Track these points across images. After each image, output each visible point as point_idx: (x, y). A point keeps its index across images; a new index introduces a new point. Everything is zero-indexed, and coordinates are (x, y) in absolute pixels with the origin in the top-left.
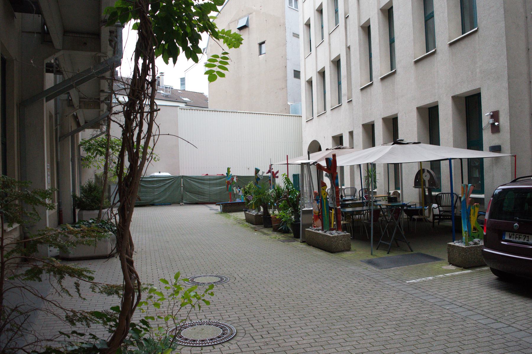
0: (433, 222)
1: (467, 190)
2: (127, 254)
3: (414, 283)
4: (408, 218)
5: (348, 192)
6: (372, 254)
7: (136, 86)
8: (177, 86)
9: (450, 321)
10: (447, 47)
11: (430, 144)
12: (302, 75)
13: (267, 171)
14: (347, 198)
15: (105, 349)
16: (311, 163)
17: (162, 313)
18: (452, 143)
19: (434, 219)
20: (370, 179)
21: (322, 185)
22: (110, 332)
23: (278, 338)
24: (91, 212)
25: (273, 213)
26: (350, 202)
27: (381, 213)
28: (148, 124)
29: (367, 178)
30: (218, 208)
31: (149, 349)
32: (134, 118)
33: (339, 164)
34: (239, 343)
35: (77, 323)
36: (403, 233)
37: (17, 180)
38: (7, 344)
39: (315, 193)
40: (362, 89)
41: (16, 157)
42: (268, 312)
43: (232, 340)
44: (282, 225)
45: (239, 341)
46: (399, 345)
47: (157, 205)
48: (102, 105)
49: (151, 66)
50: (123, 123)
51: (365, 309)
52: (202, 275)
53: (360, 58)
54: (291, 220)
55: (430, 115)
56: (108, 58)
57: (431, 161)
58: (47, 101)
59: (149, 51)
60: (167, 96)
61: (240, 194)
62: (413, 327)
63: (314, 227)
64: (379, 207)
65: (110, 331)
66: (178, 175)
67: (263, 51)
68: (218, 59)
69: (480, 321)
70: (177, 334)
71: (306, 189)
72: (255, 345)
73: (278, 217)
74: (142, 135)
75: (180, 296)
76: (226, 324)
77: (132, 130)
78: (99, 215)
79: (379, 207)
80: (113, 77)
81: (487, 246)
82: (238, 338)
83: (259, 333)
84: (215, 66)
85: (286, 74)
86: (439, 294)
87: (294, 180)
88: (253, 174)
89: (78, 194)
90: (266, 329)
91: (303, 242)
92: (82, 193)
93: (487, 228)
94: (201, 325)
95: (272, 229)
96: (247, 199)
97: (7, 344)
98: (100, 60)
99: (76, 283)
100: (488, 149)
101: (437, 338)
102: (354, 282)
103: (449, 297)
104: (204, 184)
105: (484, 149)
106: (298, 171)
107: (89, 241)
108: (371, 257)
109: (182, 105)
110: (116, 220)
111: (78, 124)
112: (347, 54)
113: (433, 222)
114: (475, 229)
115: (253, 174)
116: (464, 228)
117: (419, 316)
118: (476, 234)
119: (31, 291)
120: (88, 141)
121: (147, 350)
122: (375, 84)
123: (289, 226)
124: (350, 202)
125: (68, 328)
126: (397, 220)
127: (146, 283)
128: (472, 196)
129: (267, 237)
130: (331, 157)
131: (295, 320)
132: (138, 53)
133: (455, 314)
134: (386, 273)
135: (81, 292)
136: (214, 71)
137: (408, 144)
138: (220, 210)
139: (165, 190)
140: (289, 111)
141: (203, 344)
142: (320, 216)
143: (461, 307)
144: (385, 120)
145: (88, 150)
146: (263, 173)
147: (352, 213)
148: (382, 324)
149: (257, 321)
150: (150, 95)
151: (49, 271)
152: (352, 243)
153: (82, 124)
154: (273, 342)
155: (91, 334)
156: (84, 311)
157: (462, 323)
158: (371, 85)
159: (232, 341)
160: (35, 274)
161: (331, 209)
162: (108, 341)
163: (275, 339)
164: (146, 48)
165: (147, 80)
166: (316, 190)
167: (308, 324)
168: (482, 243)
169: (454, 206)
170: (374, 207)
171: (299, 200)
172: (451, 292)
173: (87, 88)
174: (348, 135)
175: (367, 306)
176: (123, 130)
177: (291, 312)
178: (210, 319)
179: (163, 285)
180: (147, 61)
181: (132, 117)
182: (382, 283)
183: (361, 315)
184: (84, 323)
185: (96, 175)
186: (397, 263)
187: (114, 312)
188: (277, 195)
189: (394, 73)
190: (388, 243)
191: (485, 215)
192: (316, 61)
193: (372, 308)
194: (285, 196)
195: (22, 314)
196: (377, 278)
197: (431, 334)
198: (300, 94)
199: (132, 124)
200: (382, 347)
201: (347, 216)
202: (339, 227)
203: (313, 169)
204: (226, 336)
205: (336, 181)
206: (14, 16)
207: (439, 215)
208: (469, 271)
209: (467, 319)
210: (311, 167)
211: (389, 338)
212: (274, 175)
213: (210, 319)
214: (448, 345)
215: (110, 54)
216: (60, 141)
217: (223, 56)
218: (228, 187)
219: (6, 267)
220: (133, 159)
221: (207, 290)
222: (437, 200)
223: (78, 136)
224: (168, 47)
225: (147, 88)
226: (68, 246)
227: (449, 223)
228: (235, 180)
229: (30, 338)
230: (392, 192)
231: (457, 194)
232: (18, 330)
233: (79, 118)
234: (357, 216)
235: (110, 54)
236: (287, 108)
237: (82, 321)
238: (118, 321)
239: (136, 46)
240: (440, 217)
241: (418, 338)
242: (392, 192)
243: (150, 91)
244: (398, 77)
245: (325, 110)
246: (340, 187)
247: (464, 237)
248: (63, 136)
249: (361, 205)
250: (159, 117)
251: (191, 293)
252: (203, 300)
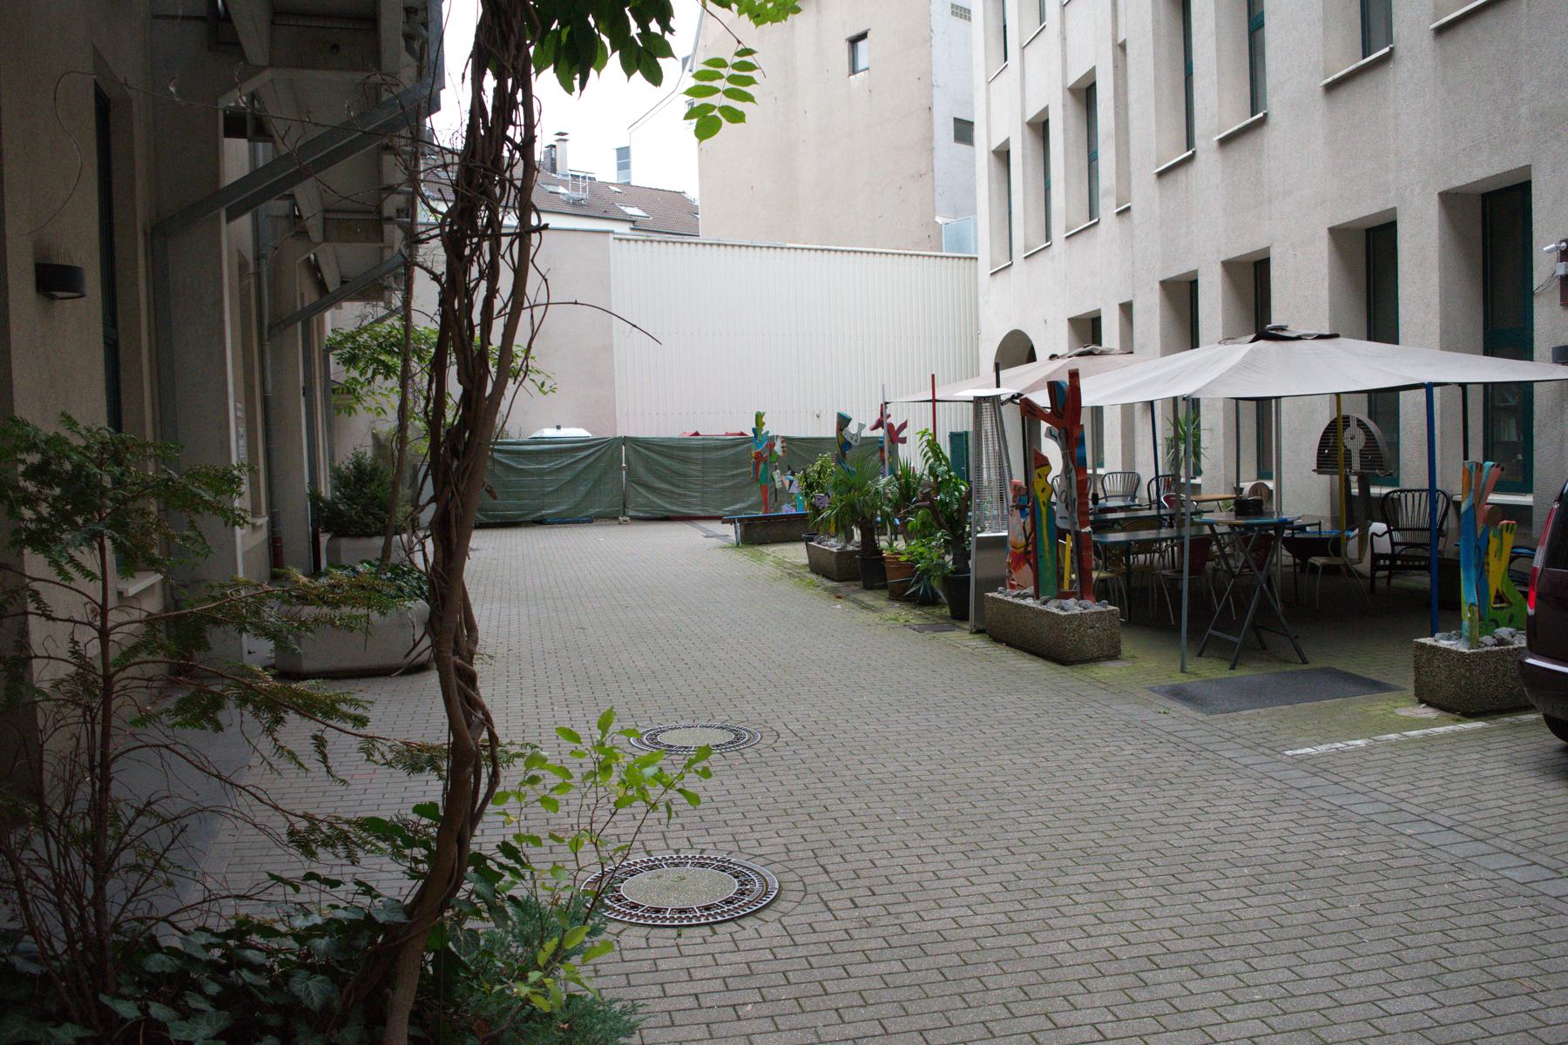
0: (1373, 577)
1: (1479, 478)
2: (456, 652)
3: (1309, 757)
4: (1295, 564)
5: (1114, 485)
6: (1183, 670)
7: (478, 157)
8: (607, 173)
9: (1416, 871)
10: (1427, 39)
11: (1369, 339)
12: (979, 133)
13: (874, 422)
14: (1111, 504)
15: (400, 925)
16: (1003, 398)
17: (566, 831)
18: (1437, 338)
19: (1375, 566)
20: (1182, 447)
21: (1036, 462)
22: (412, 878)
23: (900, 909)
24: (364, 543)
25: (891, 545)
26: (1121, 515)
27: (1215, 548)
28: (515, 270)
29: (1174, 443)
30: (730, 531)
31: (528, 929)
32: (473, 252)
33: (1088, 400)
34: (786, 921)
35: (320, 851)
36: (1279, 608)
37: (150, 439)
38: (124, 907)
39: (1016, 488)
40: (1161, 174)
41: (146, 385)
42: (872, 833)
43: (767, 912)
44: (917, 582)
45: (785, 914)
46: (1258, 937)
47: (552, 523)
48: (387, 228)
49: (519, 97)
50: (441, 268)
51: (1158, 829)
52: (682, 723)
53: (1156, 80)
54: (944, 566)
55: (1370, 253)
56: (401, 89)
57: (1369, 392)
58: (229, 220)
59: (513, 52)
60: (576, 203)
61: (794, 490)
62: (1303, 884)
63: (1012, 587)
64: (1207, 530)
65: (413, 874)
66: (611, 436)
67: (862, 62)
68: (723, 71)
69: (1507, 873)
70: (604, 892)
71: (988, 474)
72: (834, 925)
73: (903, 558)
74: (498, 304)
75: (614, 779)
76: (749, 864)
77: (467, 289)
78: (386, 550)
79: (1207, 530)
80: (421, 139)
81: (1535, 649)
82: (783, 906)
83: (846, 894)
84: (715, 91)
85: (931, 129)
86: (1387, 790)
87: (953, 451)
88: (831, 432)
89: (326, 490)
90: (867, 882)
91: (979, 632)
92: (335, 488)
93: (1539, 596)
94: (676, 865)
95: (886, 593)
96: (813, 506)
97: (124, 907)
98: (378, 96)
99: (315, 737)
100: (1549, 354)
101: (1373, 920)
102: (1129, 750)
103: (1415, 801)
104: (685, 461)
105: (1536, 354)
106: (965, 423)
107: (349, 617)
108: (1179, 679)
109: (623, 229)
110: (425, 555)
111: (321, 286)
112: (1116, 67)
113: (1373, 577)
114: (1500, 597)
115: (831, 432)
116: (1468, 595)
117: (1323, 853)
118: (1504, 614)
119: (192, 757)
120: (351, 337)
121: (521, 932)
122: (1201, 157)
123: (936, 584)
124: (1121, 515)
125: (293, 864)
126: (1260, 568)
127: (519, 741)
128: (1494, 498)
129: (872, 617)
130: (1065, 379)
131: (949, 857)
132: (482, 58)
133: (1431, 852)
134: (1224, 726)
135: (331, 762)
136: (714, 107)
137: (1299, 338)
138: (733, 537)
140: (939, 244)
141: (683, 919)
142: (1028, 555)
143: (1450, 828)
144: (1230, 267)
145: (351, 361)
146: (861, 426)
147: (1126, 548)
148: (1209, 876)
149: (839, 859)
150: (518, 183)
151: (243, 701)
152: (1122, 636)
153: (332, 283)
154: (886, 920)
155: (359, 883)
156: (338, 818)
157: (1451, 877)
158: (1190, 159)
159: (746, 923)
160: (203, 711)
161: (1062, 534)
162: (408, 901)
163: (892, 910)
164: (506, 42)
165: (509, 139)
166: (1019, 477)
167: (988, 869)
168: (1521, 641)
169: (1436, 531)
170: (1194, 531)
171: (968, 508)
172: (1420, 784)
173: (344, 178)
174: (1116, 312)
175: (1165, 821)
176: (443, 292)
177: (938, 834)
178: (703, 851)
179: (568, 746)
180: (510, 81)
181: (467, 251)
182: (1211, 756)
183: (1145, 846)
184: (340, 849)
185: (375, 437)
186: (1255, 696)
187: (425, 821)
188: (901, 493)
189: (1262, 122)
190: (1231, 638)
191: (1532, 557)
192: (1023, 91)
193: (1182, 828)
194: (926, 497)
195: (165, 821)
196: (1198, 741)
197: (1355, 907)
198: (971, 192)
199: (466, 271)
200: (1208, 942)
201: (1110, 554)
202: (1085, 589)
203: (1011, 416)
204: (748, 900)
205: (1077, 452)
207: (1392, 557)
208: (1479, 724)
209: (1468, 867)
210: (1003, 408)
211: (1228, 917)
212: (895, 436)
213: (703, 851)
214: (1407, 940)
215: (407, 75)
217: (738, 59)
218: (756, 469)
219: (117, 688)
220: (473, 375)
221: (691, 762)
222: (1387, 510)
223: (321, 323)
224: (570, 35)
225: (511, 166)
226: (289, 632)
227: (1421, 581)
228: (778, 448)
229: (194, 894)
230: (1247, 486)
231: (1448, 492)
232: (154, 865)
233: (325, 269)
234: (1141, 557)
235: (407, 75)
236: (934, 235)
237: (334, 846)
238: (434, 845)
239: (477, 36)
240: (1393, 563)
241: (1315, 917)
242: (1247, 486)
243: (518, 172)
244: (1272, 136)
245: (1048, 238)
246: (1090, 471)
247: (1466, 623)
248: (279, 322)
249: (1154, 522)
250: (545, 251)
251: (648, 772)
252: (680, 791)
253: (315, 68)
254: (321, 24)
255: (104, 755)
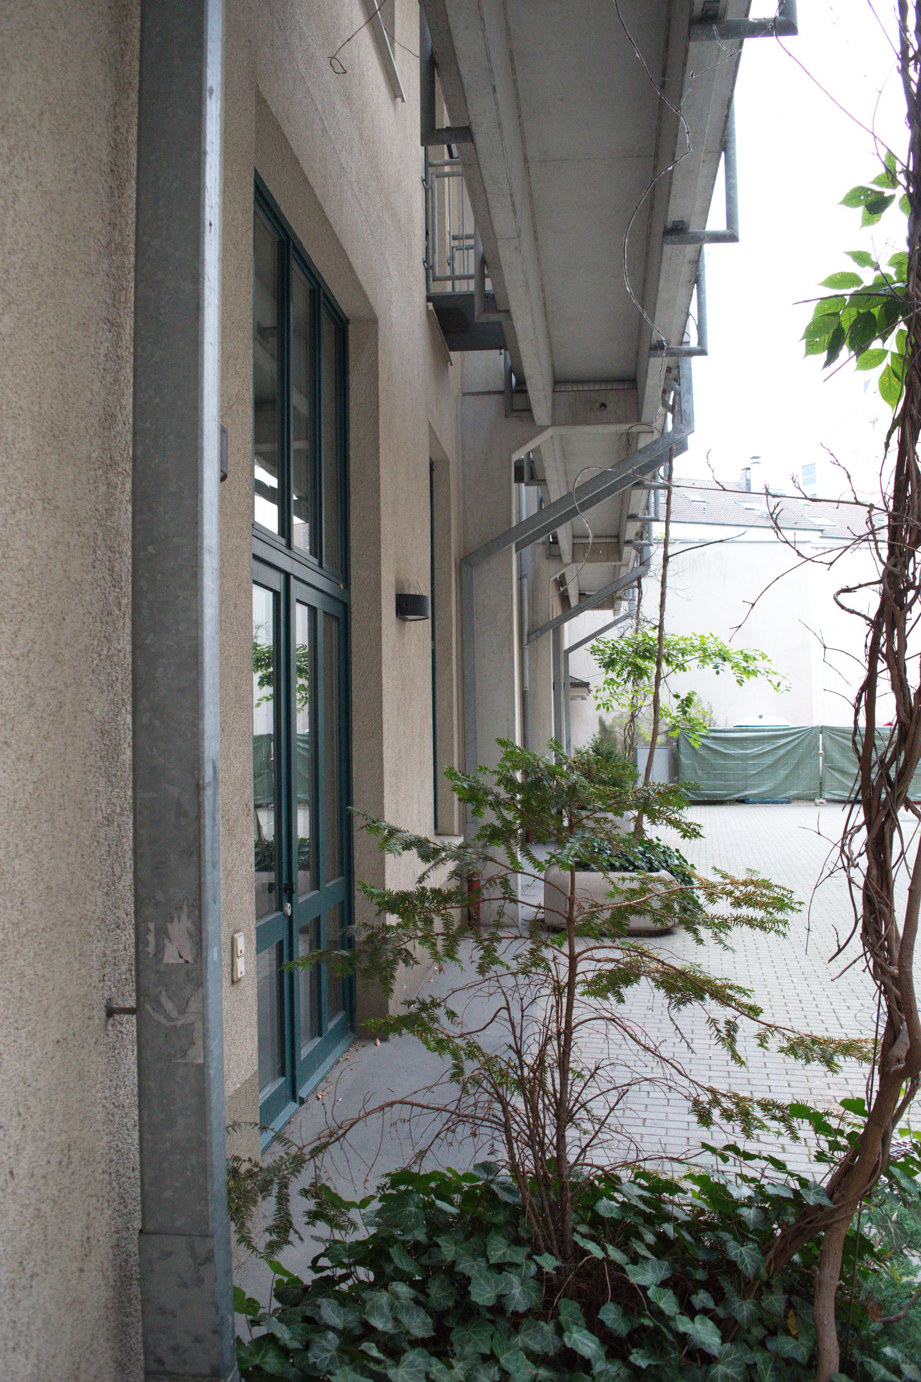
139: (776, 762)
206: (448, 360)
216: (528, 642)
248: (541, 631)
253: (588, 424)
254: (603, 387)
255: (568, 1022)
